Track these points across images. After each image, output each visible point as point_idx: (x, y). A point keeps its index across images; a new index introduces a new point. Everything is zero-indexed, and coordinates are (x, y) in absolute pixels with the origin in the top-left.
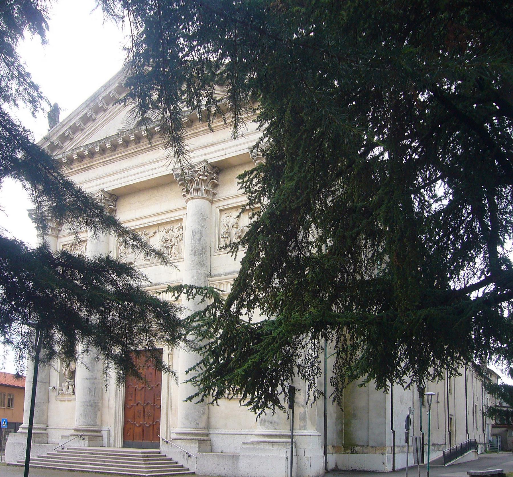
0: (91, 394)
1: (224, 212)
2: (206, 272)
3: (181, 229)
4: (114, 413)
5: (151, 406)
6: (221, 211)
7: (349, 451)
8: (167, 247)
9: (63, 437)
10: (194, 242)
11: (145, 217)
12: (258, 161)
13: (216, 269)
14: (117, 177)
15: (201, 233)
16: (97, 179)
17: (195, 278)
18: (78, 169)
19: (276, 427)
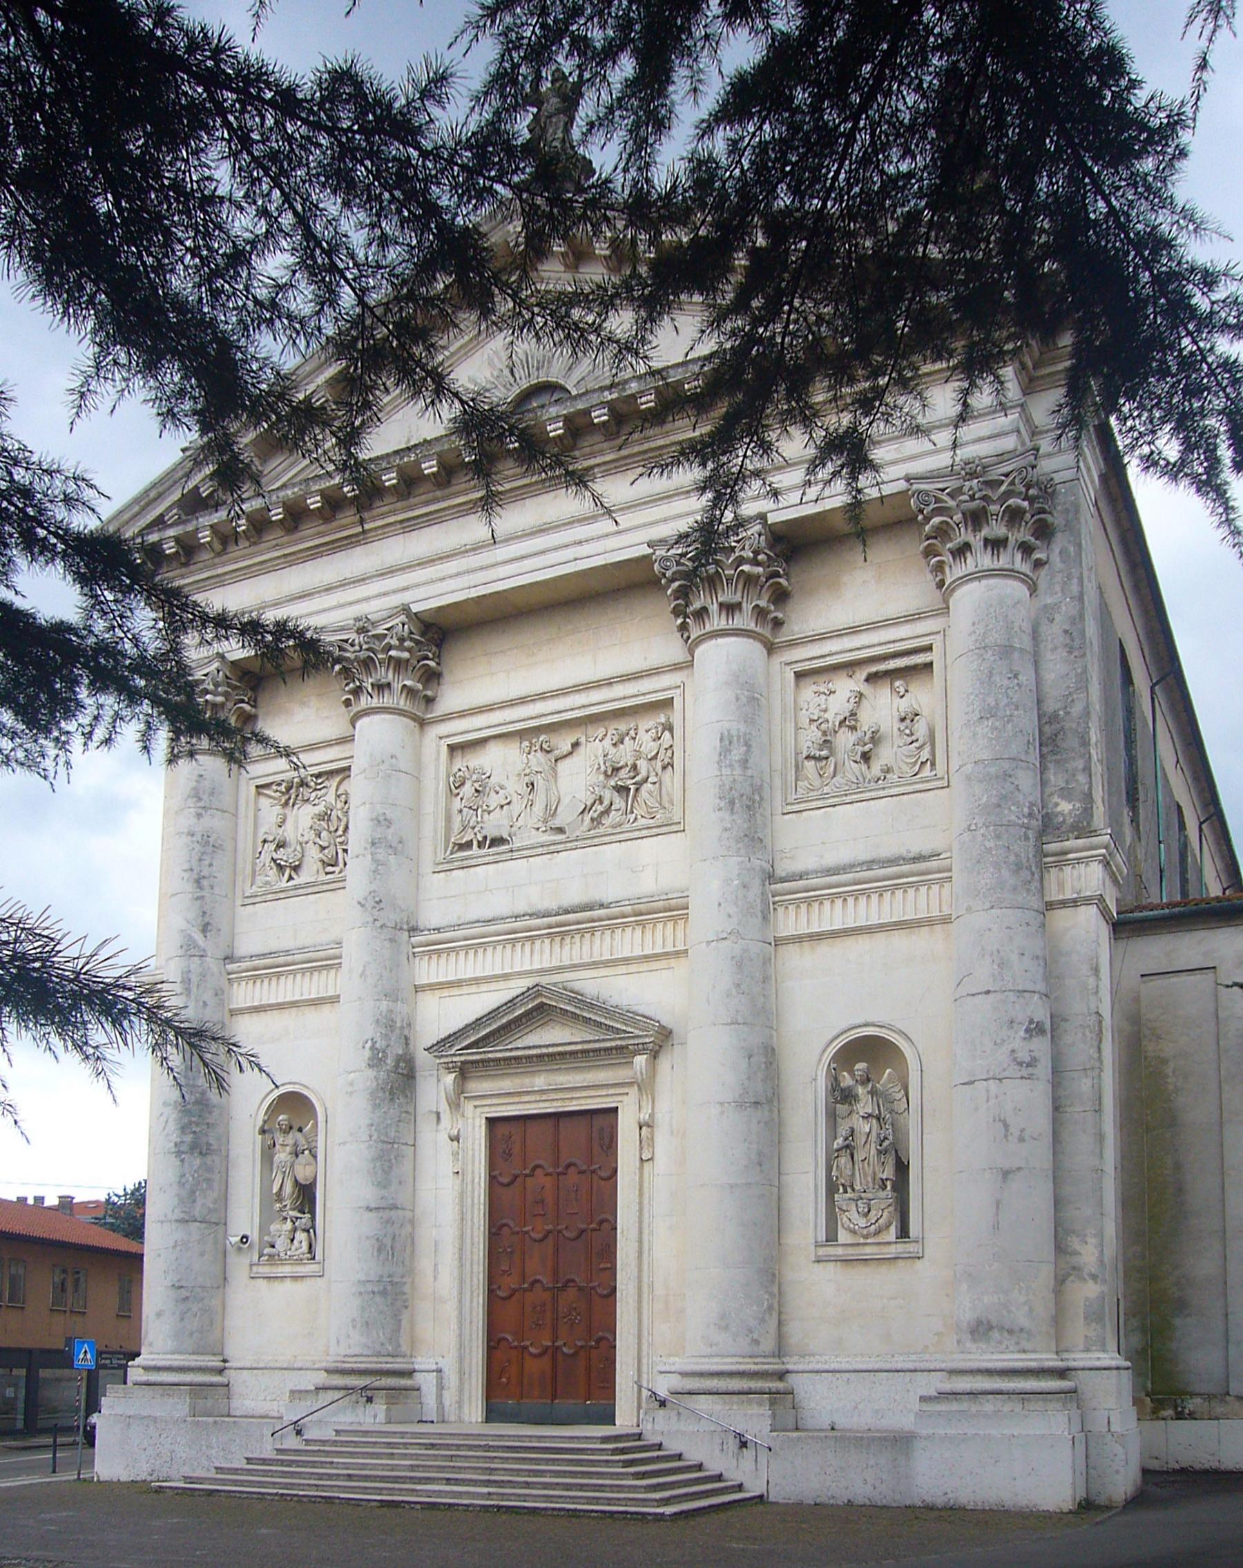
0: (383, 1255)
1: (809, 680)
2: (765, 865)
3: (667, 733)
4: (454, 1314)
5: (580, 1289)
6: (799, 676)
7: (1169, 1412)
8: (622, 790)
9: (296, 1394)
10: (727, 771)
11: (541, 697)
12: (936, 520)
13: (792, 858)
14: (452, 566)
15: (747, 745)
16: (382, 574)
17: (736, 882)
18: (317, 542)
19: (1025, 1345)
